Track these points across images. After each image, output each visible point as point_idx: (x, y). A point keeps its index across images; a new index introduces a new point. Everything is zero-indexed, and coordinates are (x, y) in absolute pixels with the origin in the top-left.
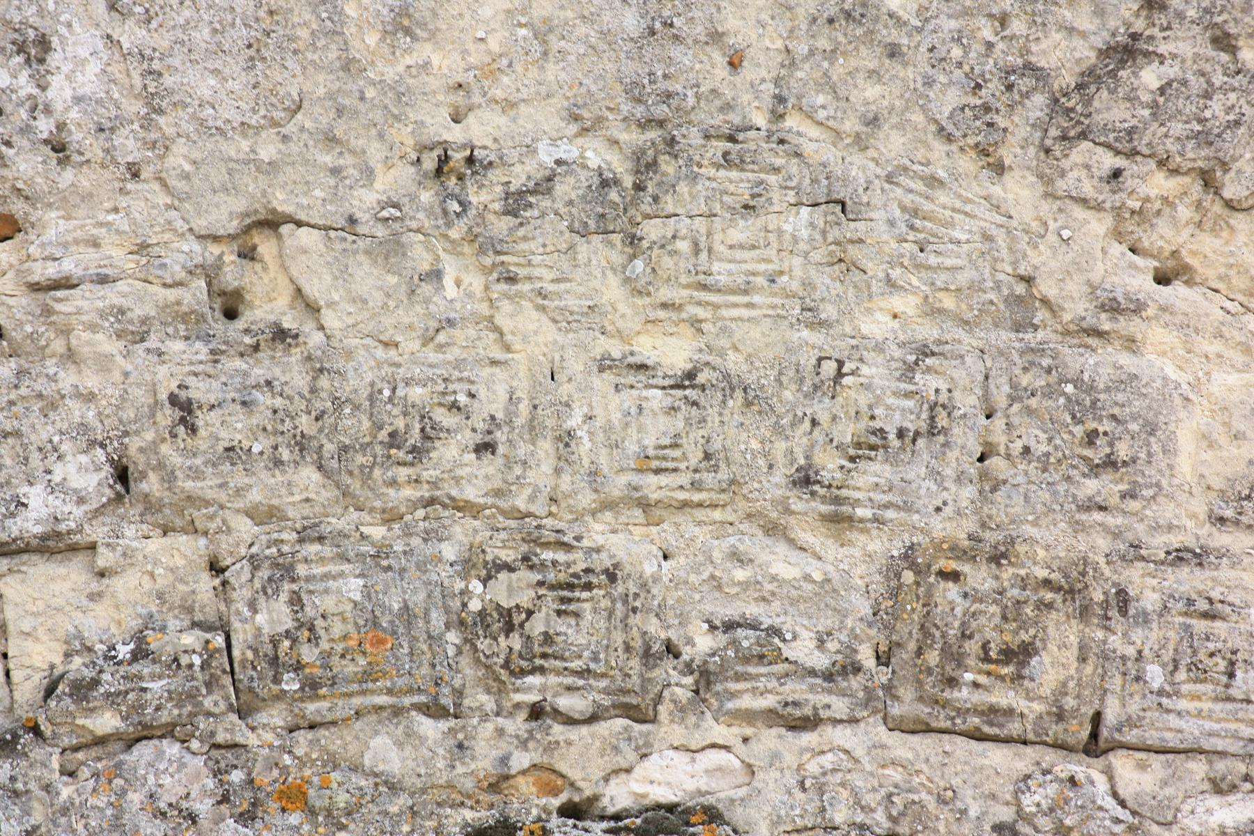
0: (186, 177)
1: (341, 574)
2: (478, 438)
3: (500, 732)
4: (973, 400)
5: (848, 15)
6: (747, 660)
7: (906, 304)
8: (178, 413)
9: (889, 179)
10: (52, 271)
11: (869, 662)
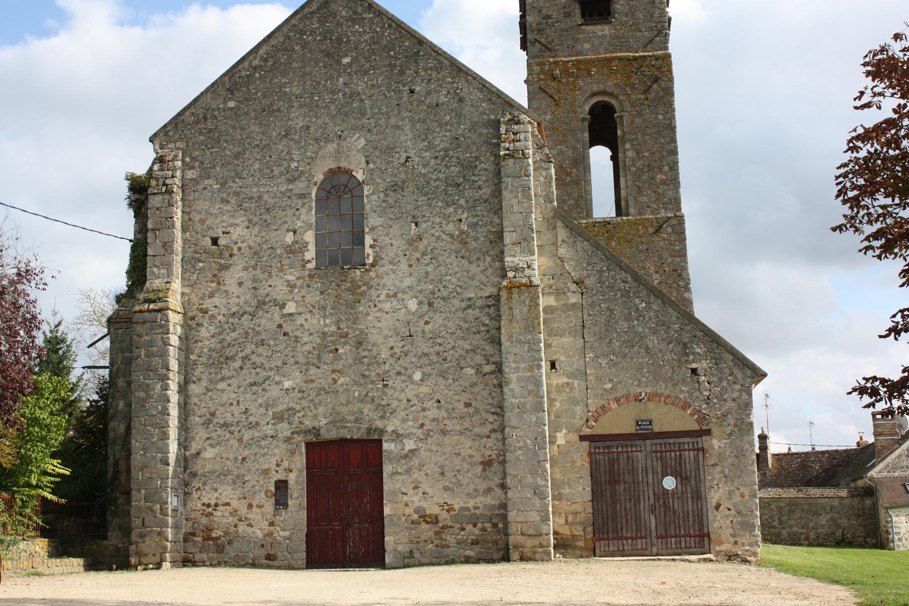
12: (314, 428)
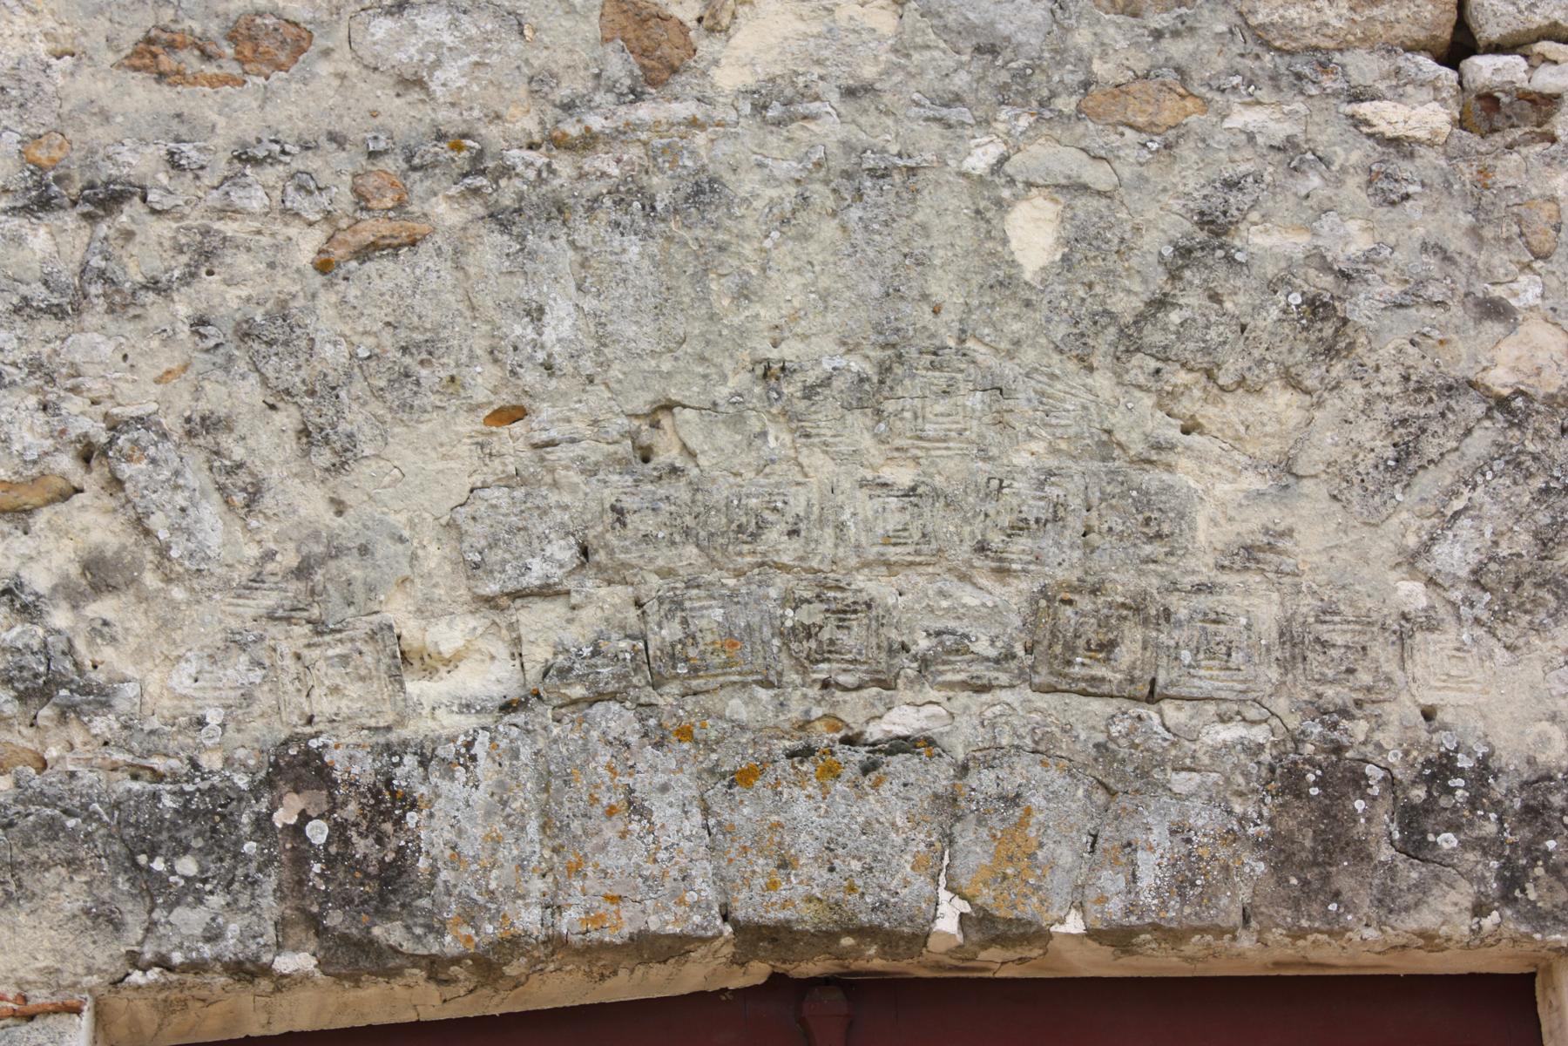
0: (620, 381)
1: (710, 607)
2: (790, 527)
3: (805, 696)
4: (1078, 501)
5: (1001, 284)
6: (949, 653)
7: (1039, 447)
8: (616, 516)
9: (1027, 375)
10: (544, 436)
11: (1021, 653)
12: (300, 766)
